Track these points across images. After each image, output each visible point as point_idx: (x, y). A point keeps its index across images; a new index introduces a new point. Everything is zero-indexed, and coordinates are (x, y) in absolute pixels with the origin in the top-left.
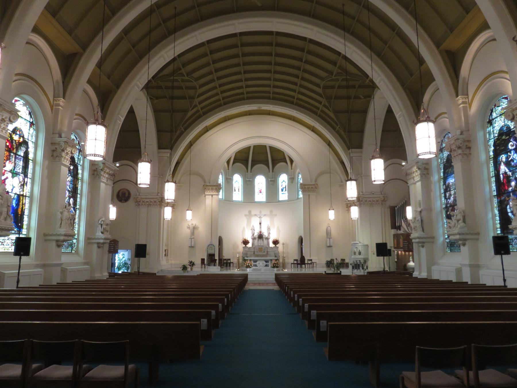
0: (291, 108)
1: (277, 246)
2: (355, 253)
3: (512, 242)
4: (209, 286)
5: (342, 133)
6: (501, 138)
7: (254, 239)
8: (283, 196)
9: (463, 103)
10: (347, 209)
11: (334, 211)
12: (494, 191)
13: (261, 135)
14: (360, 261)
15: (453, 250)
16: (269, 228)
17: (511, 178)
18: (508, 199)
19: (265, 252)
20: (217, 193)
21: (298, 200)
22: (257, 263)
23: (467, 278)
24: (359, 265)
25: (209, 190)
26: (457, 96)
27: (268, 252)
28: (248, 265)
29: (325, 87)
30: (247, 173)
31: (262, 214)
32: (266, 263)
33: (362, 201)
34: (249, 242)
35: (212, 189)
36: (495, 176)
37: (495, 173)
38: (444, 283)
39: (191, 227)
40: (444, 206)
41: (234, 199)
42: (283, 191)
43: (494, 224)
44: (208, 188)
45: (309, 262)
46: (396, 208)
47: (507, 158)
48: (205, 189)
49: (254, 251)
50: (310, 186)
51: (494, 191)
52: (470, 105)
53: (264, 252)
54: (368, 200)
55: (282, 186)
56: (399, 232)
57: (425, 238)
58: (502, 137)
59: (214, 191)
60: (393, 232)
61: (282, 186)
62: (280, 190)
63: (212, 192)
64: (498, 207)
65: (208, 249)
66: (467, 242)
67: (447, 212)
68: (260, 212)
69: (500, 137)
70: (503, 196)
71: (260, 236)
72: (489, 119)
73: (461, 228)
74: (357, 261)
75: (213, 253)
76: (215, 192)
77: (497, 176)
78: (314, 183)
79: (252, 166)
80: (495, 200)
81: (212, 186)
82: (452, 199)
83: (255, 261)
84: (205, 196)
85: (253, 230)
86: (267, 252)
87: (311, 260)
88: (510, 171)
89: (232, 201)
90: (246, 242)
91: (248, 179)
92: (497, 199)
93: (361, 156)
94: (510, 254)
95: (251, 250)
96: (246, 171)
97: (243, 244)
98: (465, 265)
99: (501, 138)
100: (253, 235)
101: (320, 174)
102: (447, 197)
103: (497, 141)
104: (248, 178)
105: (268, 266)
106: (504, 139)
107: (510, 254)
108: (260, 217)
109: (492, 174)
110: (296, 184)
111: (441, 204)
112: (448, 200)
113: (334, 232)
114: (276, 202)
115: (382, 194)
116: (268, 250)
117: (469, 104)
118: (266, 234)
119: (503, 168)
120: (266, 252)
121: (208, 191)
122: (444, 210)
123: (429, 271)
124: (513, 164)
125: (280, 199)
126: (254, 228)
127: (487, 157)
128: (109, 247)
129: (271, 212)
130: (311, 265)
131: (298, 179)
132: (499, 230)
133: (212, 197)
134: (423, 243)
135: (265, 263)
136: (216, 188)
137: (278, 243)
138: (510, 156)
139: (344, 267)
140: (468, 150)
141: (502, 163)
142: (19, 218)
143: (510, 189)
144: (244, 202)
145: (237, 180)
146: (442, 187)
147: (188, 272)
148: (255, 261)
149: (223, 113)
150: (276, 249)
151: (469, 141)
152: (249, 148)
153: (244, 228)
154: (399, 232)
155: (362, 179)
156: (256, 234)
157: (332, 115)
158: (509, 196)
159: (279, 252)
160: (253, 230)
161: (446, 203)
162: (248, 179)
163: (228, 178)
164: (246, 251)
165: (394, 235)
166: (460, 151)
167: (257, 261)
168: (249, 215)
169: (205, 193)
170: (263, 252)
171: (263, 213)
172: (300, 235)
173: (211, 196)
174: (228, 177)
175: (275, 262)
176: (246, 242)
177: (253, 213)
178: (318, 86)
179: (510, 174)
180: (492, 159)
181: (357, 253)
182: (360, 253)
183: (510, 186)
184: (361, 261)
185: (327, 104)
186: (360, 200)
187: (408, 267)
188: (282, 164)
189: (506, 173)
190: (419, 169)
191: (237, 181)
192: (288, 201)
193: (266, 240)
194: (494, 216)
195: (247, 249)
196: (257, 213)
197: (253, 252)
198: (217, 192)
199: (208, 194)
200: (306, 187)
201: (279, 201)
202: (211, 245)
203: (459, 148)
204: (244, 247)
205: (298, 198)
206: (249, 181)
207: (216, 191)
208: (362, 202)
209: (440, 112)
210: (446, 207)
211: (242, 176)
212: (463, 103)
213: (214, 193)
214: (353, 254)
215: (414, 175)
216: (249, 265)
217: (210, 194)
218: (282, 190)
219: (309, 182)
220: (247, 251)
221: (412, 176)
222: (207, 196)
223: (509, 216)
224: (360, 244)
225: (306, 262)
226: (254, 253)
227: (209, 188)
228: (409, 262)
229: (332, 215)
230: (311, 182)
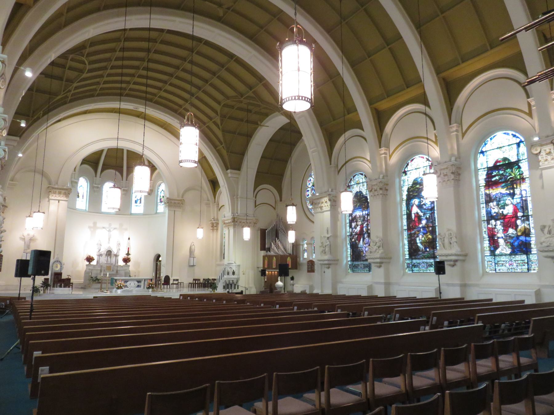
0: (169, 114)
1: (128, 264)
2: (228, 274)
3: (420, 265)
4: (219, 307)
5: (224, 152)
6: (415, 187)
7: (100, 255)
8: (137, 209)
9: (385, 153)
10: (212, 228)
11: (203, 230)
12: (405, 226)
13: (135, 141)
14: (233, 280)
15: (355, 271)
16: (119, 244)
17: (423, 217)
18: (418, 233)
21: (157, 215)
22: (128, 284)
23: (380, 292)
24: (231, 285)
25: (55, 193)
26: (380, 147)
27: (118, 271)
28: (119, 285)
29: (226, 106)
30: (95, 178)
31: (112, 226)
32: (138, 283)
33: (237, 222)
35: (60, 193)
36: (407, 214)
37: (407, 212)
38: (366, 298)
39: (27, 239)
40: (348, 234)
41: (77, 207)
42: (138, 203)
43: (404, 251)
44: (54, 191)
45: (175, 282)
46: (266, 231)
47: (420, 202)
49: (101, 270)
50: (177, 202)
51: (405, 226)
52: (390, 156)
53: (113, 271)
54: (242, 222)
55: (136, 197)
56: (269, 253)
57: (332, 260)
58: (417, 185)
59: (62, 196)
60: (263, 253)
61: (136, 197)
63: (59, 196)
64: (408, 238)
66: (383, 265)
67: (351, 239)
68: (110, 225)
69: (414, 186)
70: (413, 230)
71: (109, 253)
72: (404, 170)
73: (382, 253)
74: (229, 281)
75: (59, 272)
77: (409, 215)
78: (181, 199)
79: (102, 171)
80: (406, 234)
81: (60, 189)
82: (358, 228)
83: (126, 281)
84: (49, 201)
87: (177, 280)
88: (422, 212)
89: (76, 209)
90: (90, 259)
91: (96, 186)
92: (408, 232)
93: (238, 178)
94: (16, 275)
95: (96, 269)
96: (95, 176)
98: (377, 283)
99: (415, 187)
100: (99, 250)
101: (186, 191)
102: (353, 227)
103: (411, 188)
104: (96, 184)
105: (141, 287)
106: (418, 188)
107: (16, 275)
108: (109, 231)
109: (404, 212)
110: (156, 197)
111: (346, 233)
112: (354, 229)
113: (197, 253)
114: (128, 215)
115: (254, 217)
117: (390, 156)
118: (115, 251)
119: (415, 210)
120: (115, 271)
121: (54, 195)
122: (348, 237)
123: (334, 287)
124: (425, 207)
125: (133, 212)
127: (400, 199)
128: (308, 267)
129: (121, 225)
130: (177, 285)
131: (158, 192)
132: (408, 256)
133: (59, 202)
134: (330, 264)
135: (137, 284)
136: (65, 192)
137: (129, 261)
138: (422, 201)
139: (201, 287)
140: (386, 191)
141: (415, 205)
143: (421, 226)
144: (88, 212)
145: (83, 185)
146: (347, 218)
147: (40, 295)
148: (126, 281)
149: (93, 105)
150: (126, 268)
151: (387, 184)
152: (102, 151)
154: (269, 253)
155: (237, 200)
156: (103, 250)
157: (219, 133)
158: (419, 231)
161: (351, 231)
162: (96, 186)
163: (73, 181)
164: (90, 269)
165: (264, 257)
166: (381, 192)
167: (128, 281)
168: (94, 227)
169: (48, 197)
171: (114, 226)
172: (157, 254)
173: (57, 201)
174: (73, 180)
175: (151, 282)
176: (91, 259)
177: (99, 225)
178: (219, 103)
179: (421, 214)
180: (405, 201)
181: (231, 273)
182: (234, 273)
183: (420, 223)
184: (234, 281)
185: (219, 122)
186: (235, 221)
187: (276, 286)
189: (417, 213)
190: (330, 200)
191: (81, 186)
192: (144, 214)
193: (115, 257)
194: (404, 245)
195: (91, 268)
196: (106, 225)
197: (100, 271)
199: (53, 198)
200: (173, 202)
201: (131, 214)
202: (57, 261)
203: (381, 189)
204: (87, 265)
205: (156, 213)
206: (98, 187)
207: (64, 196)
208: (237, 223)
209: (355, 155)
210: (351, 235)
211: (88, 180)
212: (385, 153)
214: (226, 273)
215: (323, 205)
216: (122, 285)
218: (136, 202)
219: (175, 197)
220: (92, 270)
221: (319, 206)
223: (418, 246)
224: (234, 265)
225: (171, 282)
228: (277, 281)
229: (200, 233)
230: (178, 197)
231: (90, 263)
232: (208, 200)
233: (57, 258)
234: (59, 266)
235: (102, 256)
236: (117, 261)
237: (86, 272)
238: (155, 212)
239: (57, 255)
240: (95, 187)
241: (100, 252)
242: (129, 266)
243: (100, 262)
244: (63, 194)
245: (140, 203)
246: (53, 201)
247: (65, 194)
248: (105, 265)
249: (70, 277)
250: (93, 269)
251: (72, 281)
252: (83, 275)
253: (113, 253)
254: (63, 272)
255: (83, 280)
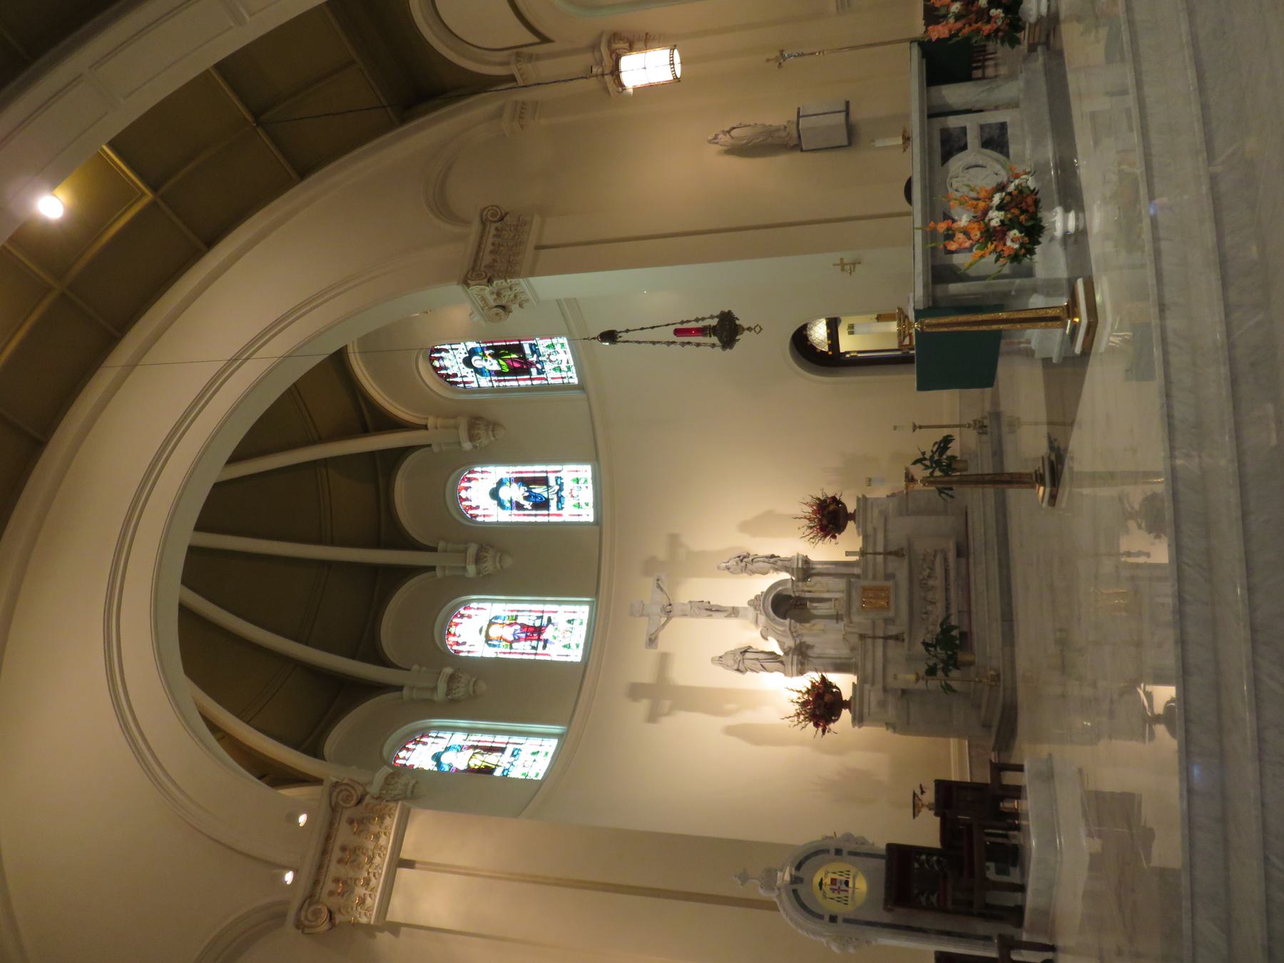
1: (851, 508)
16: (742, 558)
19: (890, 570)
20: (387, 821)
25: (347, 886)
27: (892, 548)
30: (406, 692)
34: (726, 311)
35: (352, 855)
44: (331, 893)
48: (331, 915)
49: (886, 638)
59: (370, 845)
62: (540, 517)
63: (371, 860)
65: (833, 919)
76: (377, 837)
84: (395, 928)
85: (743, 659)
86: (890, 553)
91: (442, 687)
95: (879, 666)
96: (397, 694)
97: (832, 726)
104: (434, 689)
114: (601, 533)
116: (880, 549)
121: (360, 891)
126: (733, 653)
133: (409, 864)
136: (351, 822)
142: (1151, 480)
150: (874, 514)
153: (730, 731)
159: (893, 495)
160: (748, 655)
164: (882, 704)
169: (369, 930)
170: (890, 583)
173: (403, 873)
177: (645, 673)
188: (402, 488)
195: (874, 695)
197: (891, 642)
198: (382, 818)
199: (373, 902)
200: (487, 258)
204: (858, 720)
205: (581, 387)
207: (375, 828)
213: (387, 841)
217: (378, 883)
218: (542, 504)
220: (885, 690)
222: (397, 912)
226: (898, 638)
227: (337, 881)
231: (846, 705)
232: (499, 114)
233: (769, 879)
234: (823, 874)
235: (809, 647)
236: (837, 570)
237: (902, 725)
238: (577, 394)
239: (744, 878)
240: (449, 690)
241: (780, 652)
242: (863, 501)
243: (844, 652)
244: (358, 833)
245: (544, 481)
246: (397, 902)
247: (360, 823)
248: (857, 619)
249: (929, 797)
250: (879, 686)
251: (1007, 46)
252: (920, 738)
253: (789, 590)
254: (880, 843)
255: (953, 742)
